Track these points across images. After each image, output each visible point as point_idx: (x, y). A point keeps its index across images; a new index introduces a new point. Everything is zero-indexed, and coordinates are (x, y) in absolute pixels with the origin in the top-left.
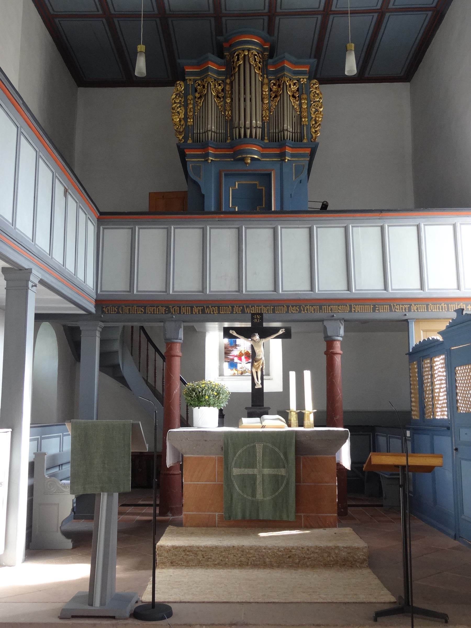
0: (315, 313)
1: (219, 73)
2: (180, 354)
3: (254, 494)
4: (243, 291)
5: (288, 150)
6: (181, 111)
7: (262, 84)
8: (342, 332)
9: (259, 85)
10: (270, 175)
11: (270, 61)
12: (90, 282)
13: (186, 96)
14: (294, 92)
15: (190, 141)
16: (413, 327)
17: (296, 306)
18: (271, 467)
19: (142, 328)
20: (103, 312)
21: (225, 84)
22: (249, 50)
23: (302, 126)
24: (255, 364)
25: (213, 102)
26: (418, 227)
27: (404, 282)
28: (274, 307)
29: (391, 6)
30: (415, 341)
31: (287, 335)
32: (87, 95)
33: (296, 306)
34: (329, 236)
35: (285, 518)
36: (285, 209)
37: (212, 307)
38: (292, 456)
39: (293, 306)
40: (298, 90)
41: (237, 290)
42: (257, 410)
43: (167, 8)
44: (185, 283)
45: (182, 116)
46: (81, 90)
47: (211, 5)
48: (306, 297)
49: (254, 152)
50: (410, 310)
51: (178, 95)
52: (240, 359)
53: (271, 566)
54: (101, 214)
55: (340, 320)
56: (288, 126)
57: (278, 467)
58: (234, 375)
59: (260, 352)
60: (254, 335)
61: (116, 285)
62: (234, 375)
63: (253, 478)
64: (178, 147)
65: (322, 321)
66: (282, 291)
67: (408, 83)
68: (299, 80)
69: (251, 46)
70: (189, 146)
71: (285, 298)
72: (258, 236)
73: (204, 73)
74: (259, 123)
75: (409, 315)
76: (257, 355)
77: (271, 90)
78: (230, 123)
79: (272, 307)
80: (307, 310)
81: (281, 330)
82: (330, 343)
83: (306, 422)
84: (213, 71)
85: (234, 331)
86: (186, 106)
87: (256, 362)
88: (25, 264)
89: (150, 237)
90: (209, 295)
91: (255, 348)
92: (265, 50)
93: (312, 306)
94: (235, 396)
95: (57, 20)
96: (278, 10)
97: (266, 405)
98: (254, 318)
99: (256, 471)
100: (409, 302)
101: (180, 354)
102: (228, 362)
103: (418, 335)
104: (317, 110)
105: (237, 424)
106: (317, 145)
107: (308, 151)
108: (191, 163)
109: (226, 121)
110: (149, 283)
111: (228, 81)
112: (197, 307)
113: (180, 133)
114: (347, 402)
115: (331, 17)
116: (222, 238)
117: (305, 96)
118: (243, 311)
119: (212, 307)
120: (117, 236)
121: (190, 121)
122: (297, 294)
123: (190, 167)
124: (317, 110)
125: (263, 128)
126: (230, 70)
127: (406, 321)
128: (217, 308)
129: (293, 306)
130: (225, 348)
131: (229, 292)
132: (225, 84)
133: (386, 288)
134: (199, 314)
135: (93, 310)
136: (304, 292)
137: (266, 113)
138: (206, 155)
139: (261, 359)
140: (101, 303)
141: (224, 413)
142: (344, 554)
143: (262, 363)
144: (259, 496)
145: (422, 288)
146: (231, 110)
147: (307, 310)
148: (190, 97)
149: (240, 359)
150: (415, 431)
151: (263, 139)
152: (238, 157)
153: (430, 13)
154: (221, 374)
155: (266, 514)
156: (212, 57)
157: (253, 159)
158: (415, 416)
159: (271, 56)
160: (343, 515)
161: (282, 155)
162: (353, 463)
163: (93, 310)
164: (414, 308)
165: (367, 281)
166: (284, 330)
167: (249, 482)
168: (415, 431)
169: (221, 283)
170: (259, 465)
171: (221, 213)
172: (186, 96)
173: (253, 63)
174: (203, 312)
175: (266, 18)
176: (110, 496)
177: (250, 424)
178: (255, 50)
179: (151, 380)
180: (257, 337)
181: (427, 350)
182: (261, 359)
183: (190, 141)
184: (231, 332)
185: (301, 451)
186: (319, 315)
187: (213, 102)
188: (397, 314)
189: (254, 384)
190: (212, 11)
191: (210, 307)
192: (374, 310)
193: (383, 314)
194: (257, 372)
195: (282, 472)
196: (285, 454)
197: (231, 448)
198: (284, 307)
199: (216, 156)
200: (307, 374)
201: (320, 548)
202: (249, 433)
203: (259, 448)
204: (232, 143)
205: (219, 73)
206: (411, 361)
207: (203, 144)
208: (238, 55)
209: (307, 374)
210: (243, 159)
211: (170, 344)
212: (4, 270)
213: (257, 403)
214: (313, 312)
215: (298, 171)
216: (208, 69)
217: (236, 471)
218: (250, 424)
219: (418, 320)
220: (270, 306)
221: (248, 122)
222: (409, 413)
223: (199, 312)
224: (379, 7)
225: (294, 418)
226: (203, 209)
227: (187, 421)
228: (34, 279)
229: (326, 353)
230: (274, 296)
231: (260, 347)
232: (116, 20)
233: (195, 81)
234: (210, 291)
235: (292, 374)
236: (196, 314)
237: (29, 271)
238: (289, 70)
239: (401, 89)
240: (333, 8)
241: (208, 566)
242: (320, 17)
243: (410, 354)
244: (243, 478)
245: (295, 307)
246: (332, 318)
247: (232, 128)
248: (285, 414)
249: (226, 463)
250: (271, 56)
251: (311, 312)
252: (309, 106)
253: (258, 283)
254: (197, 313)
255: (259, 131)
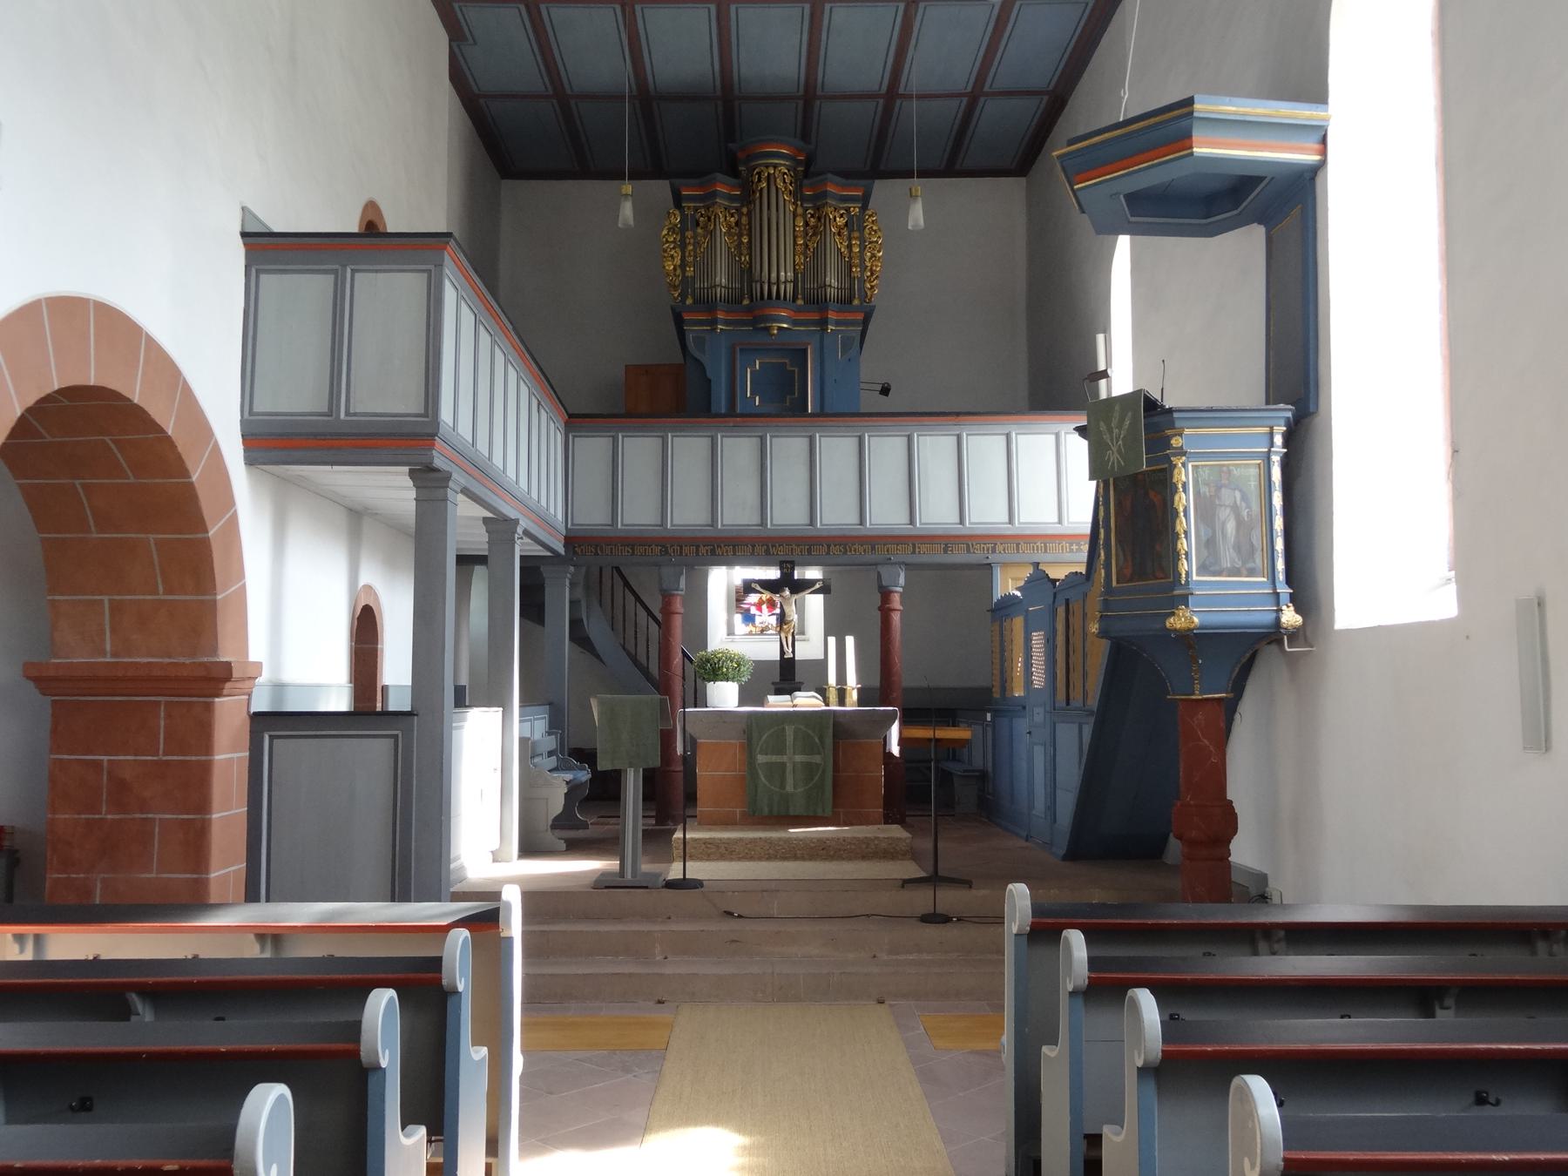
1: (732, 198)
2: (681, 610)
3: (783, 786)
5: (832, 316)
6: (677, 254)
7: (795, 215)
8: (902, 581)
9: (789, 217)
10: (805, 351)
11: (806, 182)
12: (560, 516)
13: (683, 231)
14: (840, 228)
15: (689, 301)
16: (998, 574)
18: (803, 753)
19: (618, 569)
20: (575, 553)
21: (740, 214)
22: (775, 166)
23: (852, 279)
25: (723, 241)
26: (1008, 436)
27: (987, 512)
29: (986, 89)
30: (998, 593)
31: (825, 589)
32: (515, 190)
34: (885, 448)
35: (820, 813)
36: (827, 410)
38: (829, 741)
40: (846, 224)
42: (786, 686)
43: (651, 86)
44: (688, 513)
45: (678, 261)
46: (507, 184)
47: (718, 83)
49: (782, 322)
50: (994, 551)
51: (672, 230)
52: (760, 609)
53: (803, 859)
54: (570, 416)
55: (900, 564)
56: (832, 280)
57: (812, 753)
58: (750, 633)
59: (793, 615)
61: (593, 516)
62: (750, 633)
63: (783, 765)
64: (673, 309)
65: (876, 564)
67: (1023, 180)
68: (848, 210)
69: (778, 167)
70: (689, 308)
72: (788, 448)
73: (709, 198)
74: (790, 275)
75: (992, 558)
77: (807, 224)
78: (746, 274)
82: (886, 594)
83: (848, 700)
84: (724, 196)
86: (683, 246)
88: (511, 513)
89: (639, 449)
92: (799, 163)
94: (759, 665)
95: (482, 101)
96: (819, 92)
97: (797, 679)
98: (784, 552)
99: (785, 758)
100: (993, 540)
101: (681, 610)
103: (1008, 584)
104: (873, 256)
105: (762, 703)
106: (872, 309)
107: (860, 317)
108: (692, 331)
109: (742, 271)
110: (638, 514)
111: (745, 210)
113: (675, 288)
114: (909, 676)
115: (898, 102)
116: (738, 450)
117: (856, 234)
118: (767, 552)
120: (593, 447)
121: (690, 271)
123: (690, 338)
124: (873, 256)
125: (795, 282)
126: (748, 195)
127: (989, 567)
132: (740, 214)
133: (962, 521)
135: (562, 550)
137: (800, 259)
138: (713, 322)
140: (571, 541)
142: (884, 845)
144: (789, 788)
145: (1011, 521)
146: (750, 236)
148: (689, 234)
149: (760, 609)
150: (997, 713)
151: (795, 299)
152: (758, 322)
153: (1046, 98)
154: (731, 632)
155: (798, 808)
156: (719, 176)
157: (780, 329)
158: (997, 695)
159: (806, 174)
160: (891, 815)
161: (823, 323)
162: (901, 752)
163: (562, 550)
164: (1000, 548)
165: (937, 512)
167: (777, 771)
168: (997, 713)
169: (737, 513)
170: (789, 751)
171: (736, 416)
172: (683, 231)
173: (780, 185)
174: (713, 552)
175: (801, 103)
176: (636, 772)
177: (777, 703)
178: (783, 166)
179: (630, 647)
180: (787, 592)
181: (1008, 603)
183: (689, 301)
185: (836, 733)
186: (869, 557)
187: (723, 241)
188: (977, 557)
189: (782, 652)
190: (719, 93)
192: (945, 551)
193: (958, 556)
195: (817, 759)
196: (821, 738)
197: (754, 731)
199: (726, 323)
200: (850, 641)
201: (858, 839)
202: (777, 713)
203: (789, 731)
204: (751, 302)
205: (732, 198)
206: (993, 620)
207: (707, 304)
208: (759, 174)
209: (850, 641)
210: (767, 329)
211: (667, 599)
212: (485, 520)
213: (787, 674)
215: (845, 349)
216: (714, 194)
217: (761, 759)
218: (777, 703)
219: (1005, 565)
221: (774, 275)
222: (989, 690)
224: (969, 89)
225: (833, 695)
226: (708, 409)
227: (699, 698)
228: (520, 530)
229: (881, 609)
230: (810, 532)
232: (572, 102)
233: (696, 209)
235: (832, 640)
237: (516, 522)
238: (834, 196)
239: (1011, 189)
240: (901, 91)
241: (732, 860)
242: (881, 101)
243: (992, 611)
244: (769, 765)
246: (888, 562)
247: (751, 280)
248: (822, 691)
249: (749, 748)
250: (806, 174)
252: (863, 248)
253: (788, 513)
255: (790, 287)
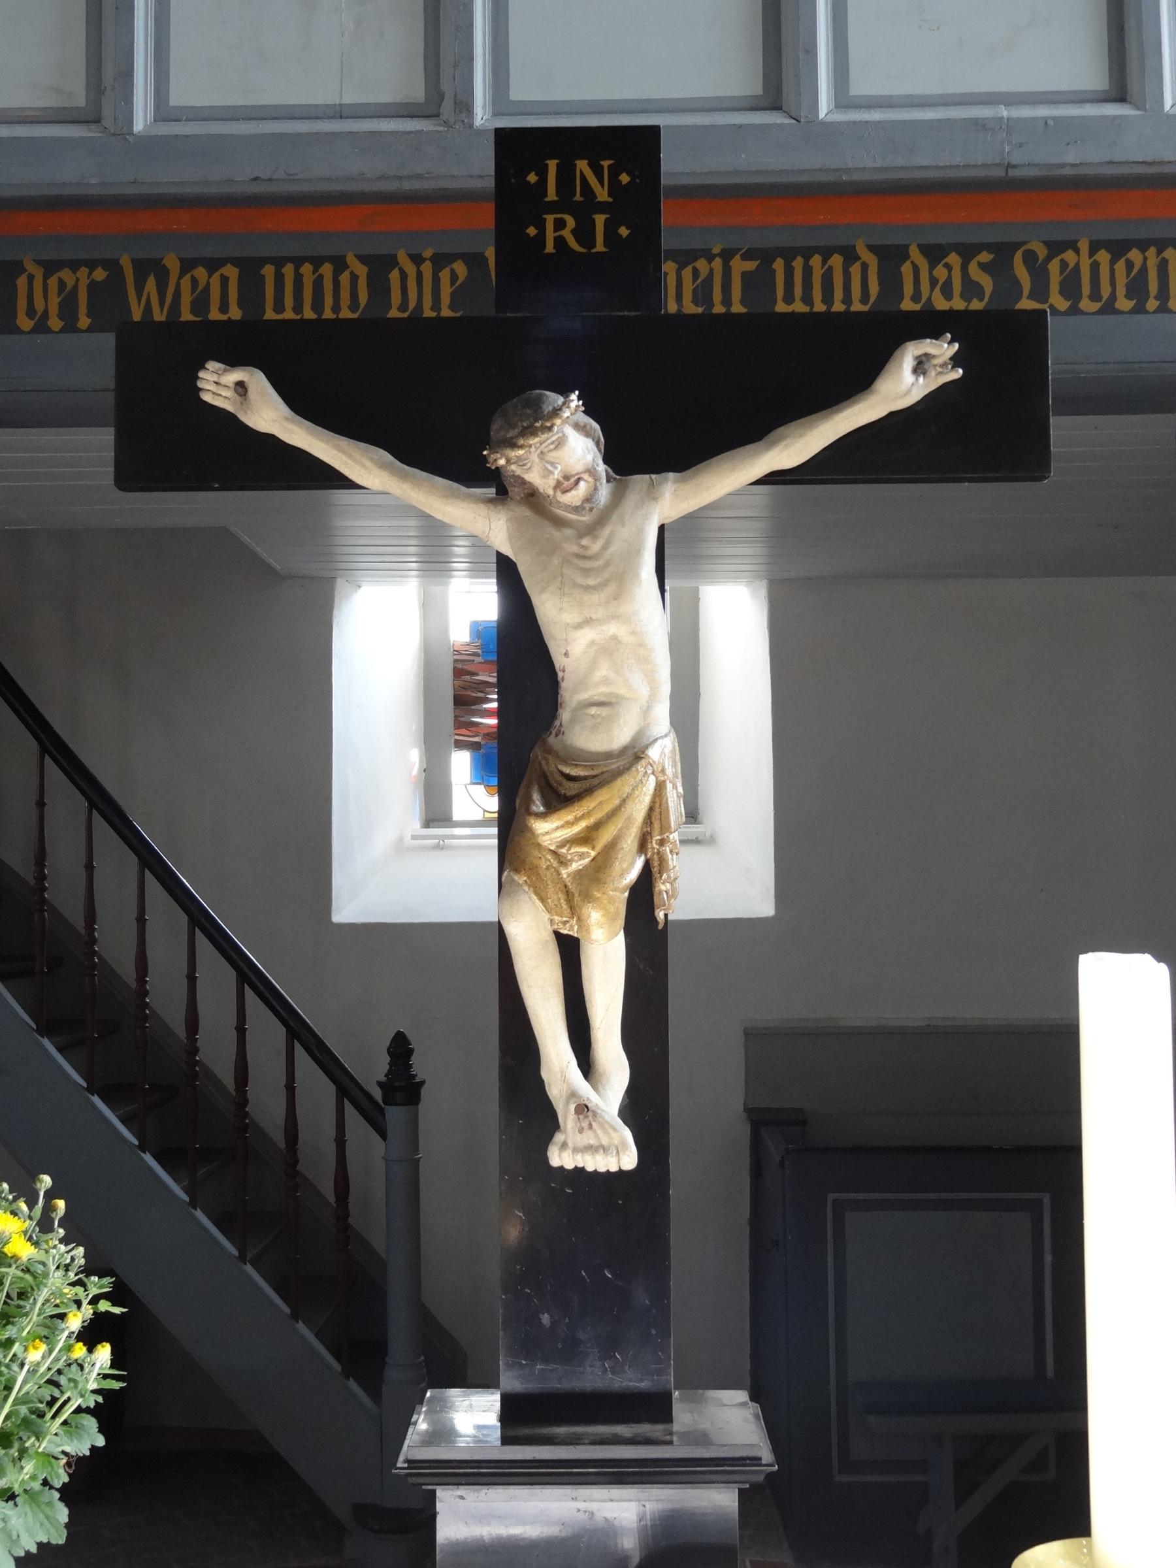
0: (1139, 309)
4: (469, 109)
17: (968, 252)
24: (549, 830)
28: (765, 256)
33: (968, 252)
37: (187, 265)
39: (935, 254)
41: (418, 93)
48: (1072, 156)
60: (536, 420)
66: (843, 100)
71: (865, 162)
76: (572, 695)
79: (739, 266)
80: (1071, 287)
81: (910, 353)
85: (257, 380)
87: (557, 801)
90: (150, 145)
91: (554, 612)
93: (1118, 249)
102: (474, 747)
112: (50, 267)
119: (187, 265)
122: (979, 125)
128: (231, 271)
129: (935, 254)
130: (458, 673)
131: (340, 112)
134: (70, 327)
136: (1043, 111)
139: (634, 754)
141: (420, 1066)
143: (638, 810)
147: (1071, 287)
166: (943, 349)
180: (567, 448)
182: (634, 754)
184: (217, 385)
191: (172, 263)
194: (570, 951)
198: (850, 255)
214: (1124, 304)
220: (727, 255)
223: (68, 309)
231: (618, 580)
234: (163, 111)
236: (41, 327)
245: (954, 259)
251: (1109, 308)
254: (55, 323)
